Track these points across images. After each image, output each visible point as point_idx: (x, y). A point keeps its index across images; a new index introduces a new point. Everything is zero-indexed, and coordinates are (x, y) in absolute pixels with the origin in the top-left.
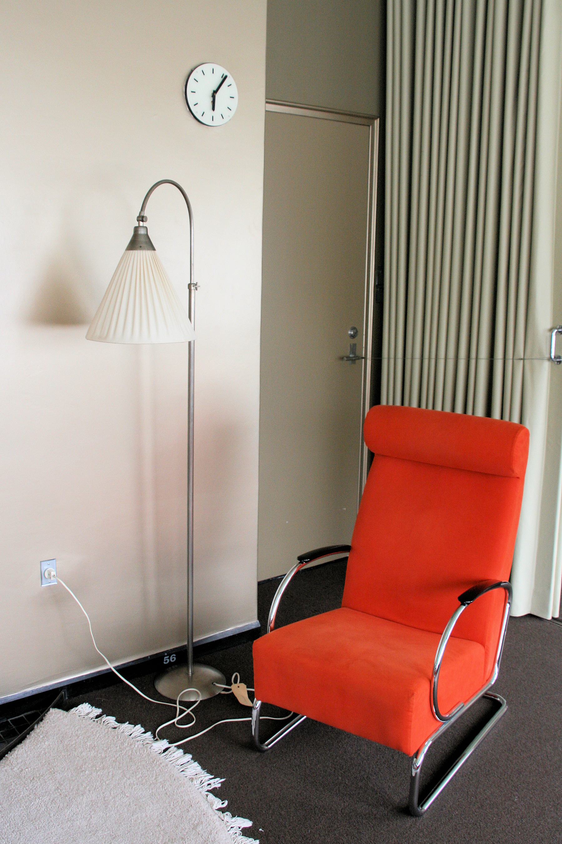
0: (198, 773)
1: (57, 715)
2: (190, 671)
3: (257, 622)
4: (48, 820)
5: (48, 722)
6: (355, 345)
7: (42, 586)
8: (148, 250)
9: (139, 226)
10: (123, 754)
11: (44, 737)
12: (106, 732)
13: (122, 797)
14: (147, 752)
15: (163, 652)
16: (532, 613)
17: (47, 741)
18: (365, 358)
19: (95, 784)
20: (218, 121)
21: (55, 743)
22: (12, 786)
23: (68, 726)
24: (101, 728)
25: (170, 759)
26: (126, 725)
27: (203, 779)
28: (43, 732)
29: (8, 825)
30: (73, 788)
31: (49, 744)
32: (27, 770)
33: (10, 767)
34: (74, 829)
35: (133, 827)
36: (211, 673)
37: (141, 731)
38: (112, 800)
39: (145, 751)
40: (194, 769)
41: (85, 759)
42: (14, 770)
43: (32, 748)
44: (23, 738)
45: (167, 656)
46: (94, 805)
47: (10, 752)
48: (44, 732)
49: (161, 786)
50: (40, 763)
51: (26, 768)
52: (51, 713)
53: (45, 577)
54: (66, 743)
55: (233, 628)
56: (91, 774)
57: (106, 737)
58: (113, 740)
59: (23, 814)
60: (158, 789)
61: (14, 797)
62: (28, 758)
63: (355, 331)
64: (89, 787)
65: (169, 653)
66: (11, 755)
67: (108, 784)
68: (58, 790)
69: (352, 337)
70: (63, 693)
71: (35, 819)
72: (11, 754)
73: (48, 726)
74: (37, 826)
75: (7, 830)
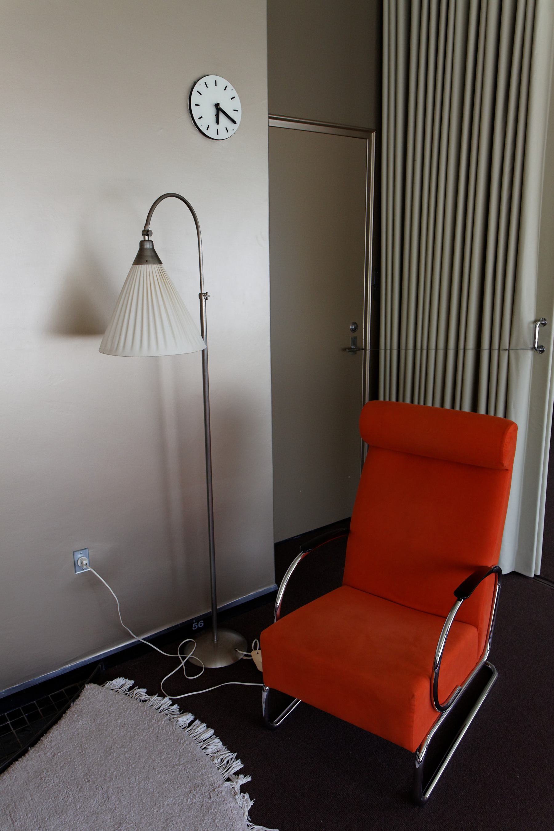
0: (220, 750)
1: (92, 691)
2: (215, 638)
3: (275, 586)
4: (74, 814)
5: (83, 699)
6: (355, 338)
7: (76, 573)
8: (154, 264)
9: (145, 240)
10: (150, 732)
11: (78, 716)
12: (136, 707)
13: (146, 783)
14: (172, 729)
15: (192, 620)
16: (516, 571)
17: (81, 720)
18: (365, 349)
19: (122, 768)
20: (223, 135)
21: (88, 722)
22: (44, 773)
23: (102, 702)
24: (132, 703)
25: (193, 734)
26: (155, 697)
27: (224, 756)
28: (78, 710)
29: (35, 820)
30: (101, 774)
31: (83, 723)
32: (59, 754)
33: (43, 752)
34: (98, 824)
35: (155, 818)
36: (234, 637)
37: (169, 703)
38: (137, 788)
39: (171, 728)
40: (215, 746)
41: (115, 738)
42: (47, 755)
43: (66, 729)
44: (60, 718)
45: (195, 622)
46: (120, 793)
47: (46, 734)
48: (79, 710)
49: (184, 768)
50: (73, 745)
51: (59, 752)
52: (87, 689)
53: (78, 565)
54: (98, 721)
55: (254, 593)
56: (118, 757)
57: (136, 713)
58: (142, 716)
59: (51, 807)
60: (180, 772)
61: (44, 786)
62: (62, 741)
63: (356, 326)
64: (116, 772)
65: (197, 620)
66: (46, 738)
67: (134, 768)
68: (87, 776)
69: (353, 331)
70: (100, 666)
71: (62, 811)
72: (46, 737)
73: (83, 703)
74: (63, 821)
75: (34, 826)
